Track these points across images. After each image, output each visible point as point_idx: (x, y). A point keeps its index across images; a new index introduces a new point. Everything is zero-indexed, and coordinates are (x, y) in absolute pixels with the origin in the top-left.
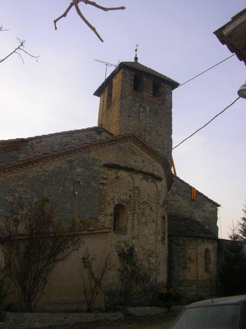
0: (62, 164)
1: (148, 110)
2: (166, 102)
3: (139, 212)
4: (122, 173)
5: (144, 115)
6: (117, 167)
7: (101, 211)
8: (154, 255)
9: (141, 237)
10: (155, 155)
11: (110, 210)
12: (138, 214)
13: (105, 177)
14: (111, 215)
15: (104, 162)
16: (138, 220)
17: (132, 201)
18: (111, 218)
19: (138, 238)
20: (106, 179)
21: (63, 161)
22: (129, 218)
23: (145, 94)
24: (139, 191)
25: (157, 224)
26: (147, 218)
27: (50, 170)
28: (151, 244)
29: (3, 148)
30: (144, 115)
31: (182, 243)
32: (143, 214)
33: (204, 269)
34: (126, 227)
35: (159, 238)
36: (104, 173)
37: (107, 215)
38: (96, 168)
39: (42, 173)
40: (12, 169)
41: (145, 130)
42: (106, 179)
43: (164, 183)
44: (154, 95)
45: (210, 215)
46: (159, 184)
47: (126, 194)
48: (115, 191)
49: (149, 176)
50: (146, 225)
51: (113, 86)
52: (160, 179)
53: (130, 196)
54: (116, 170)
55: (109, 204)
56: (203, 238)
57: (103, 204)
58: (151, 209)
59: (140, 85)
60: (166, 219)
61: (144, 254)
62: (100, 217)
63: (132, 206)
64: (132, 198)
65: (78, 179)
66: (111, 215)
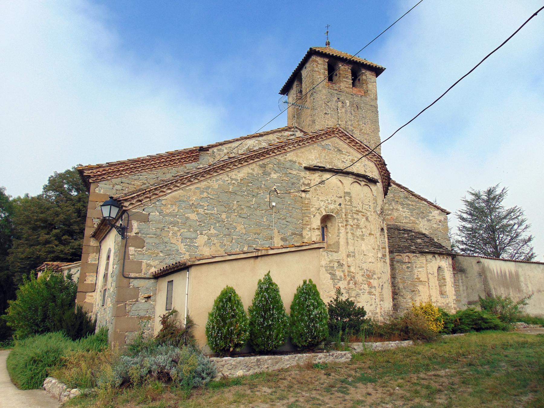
0: (253, 170)
1: (348, 104)
2: (369, 92)
3: (352, 224)
4: (327, 176)
5: (343, 110)
6: (323, 170)
7: (305, 224)
8: (375, 276)
9: (357, 255)
11: (316, 222)
12: (352, 226)
13: (306, 182)
14: (318, 229)
15: (304, 165)
16: (352, 234)
17: (344, 210)
18: (319, 233)
19: (354, 256)
20: (308, 184)
21: (254, 165)
22: (340, 231)
23: (343, 85)
24: (351, 197)
25: (376, 238)
26: (364, 230)
27: (239, 179)
28: (370, 262)
29: (178, 159)
30: (343, 110)
31: (407, 261)
32: (357, 225)
33: (438, 292)
34: (338, 243)
35: (380, 255)
36: (305, 178)
37: (314, 229)
38: (295, 173)
39: (229, 182)
40: (192, 180)
43: (380, 185)
44: (354, 85)
46: (373, 187)
47: (335, 201)
48: (321, 199)
49: (361, 179)
50: (363, 239)
51: (303, 79)
52: (373, 181)
53: (340, 205)
54: (320, 173)
55: (314, 216)
56: (434, 253)
57: (308, 217)
58: (367, 219)
59: (336, 75)
60: (386, 231)
61: (363, 275)
62: (305, 233)
63: (344, 216)
64: (343, 206)
65: (275, 187)
66: (318, 229)
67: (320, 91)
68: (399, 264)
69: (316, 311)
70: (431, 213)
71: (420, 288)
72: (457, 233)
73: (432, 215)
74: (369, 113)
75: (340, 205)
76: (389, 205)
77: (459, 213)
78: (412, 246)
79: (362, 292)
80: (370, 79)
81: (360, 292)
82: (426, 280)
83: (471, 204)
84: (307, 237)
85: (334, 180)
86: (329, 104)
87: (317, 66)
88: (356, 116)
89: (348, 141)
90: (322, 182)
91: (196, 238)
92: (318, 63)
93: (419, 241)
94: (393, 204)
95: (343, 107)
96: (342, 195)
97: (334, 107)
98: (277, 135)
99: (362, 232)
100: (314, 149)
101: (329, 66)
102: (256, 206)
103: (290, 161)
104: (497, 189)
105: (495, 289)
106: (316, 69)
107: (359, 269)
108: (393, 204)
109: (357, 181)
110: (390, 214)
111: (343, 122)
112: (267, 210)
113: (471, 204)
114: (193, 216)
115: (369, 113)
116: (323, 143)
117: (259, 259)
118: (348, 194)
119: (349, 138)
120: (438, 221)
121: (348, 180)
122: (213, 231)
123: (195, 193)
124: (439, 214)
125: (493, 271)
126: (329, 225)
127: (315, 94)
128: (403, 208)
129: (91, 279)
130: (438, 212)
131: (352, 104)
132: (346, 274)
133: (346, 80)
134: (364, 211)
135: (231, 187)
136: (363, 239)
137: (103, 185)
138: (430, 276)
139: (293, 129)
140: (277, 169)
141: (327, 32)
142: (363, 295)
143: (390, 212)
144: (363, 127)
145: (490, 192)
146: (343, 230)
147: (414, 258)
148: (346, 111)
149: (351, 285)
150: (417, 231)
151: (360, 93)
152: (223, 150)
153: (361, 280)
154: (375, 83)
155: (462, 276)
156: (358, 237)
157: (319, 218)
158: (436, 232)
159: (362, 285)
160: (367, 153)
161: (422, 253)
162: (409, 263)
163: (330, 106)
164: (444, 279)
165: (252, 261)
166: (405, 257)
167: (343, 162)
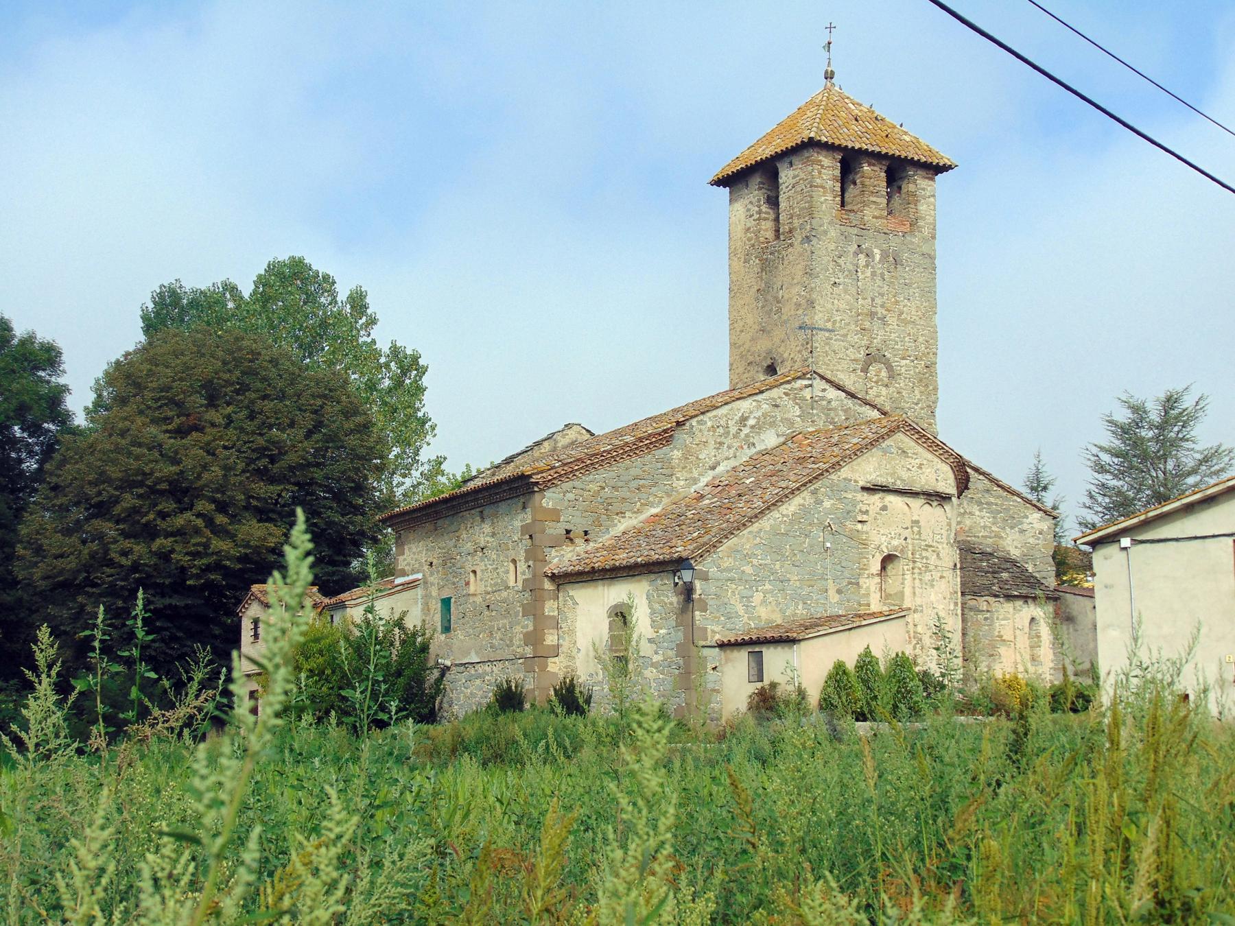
1: (878, 257)
2: (921, 223)
4: (891, 499)
7: (862, 569)
10: (941, 452)
12: (920, 569)
13: (864, 509)
15: (861, 483)
16: (921, 580)
17: (910, 547)
19: (922, 611)
20: (867, 512)
23: (869, 213)
24: (919, 527)
31: (985, 608)
34: (902, 593)
41: (872, 315)
42: (867, 512)
45: (1038, 539)
48: (882, 532)
50: (932, 586)
53: (906, 539)
54: (880, 495)
55: (873, 556)
62: (861, 581)
63: (910, 555)
64: (909, 541)
67: (825, 232)
68: (972, 613)
69: (912, 684)
70: (1027, 518)
71: (1002, 650)
72: (1084, 504)
75: (906, 539)
77: (1095, 450)
78: (993, 584)
81: (927, 659)
82: (1012, 638)
83: (1124, 431)
84: (865, 586)
85: (893, 500)
86: (840, 261)
87: (820, 173)
88: (892, 282)
89: (917, 436)
90: (884, 508)
91: (752, 597)
92: (822, 166)
93: (1005, 575)
95: (867, 266)
96: (909, 524)
97: (851, 267)
100: (872, 456)
101: (842, 162)
102: (809, 549)
103: (845, 479)
104: (1185, 398)
106: (818, 180)
112: (821, 553)
113: (1124, 431)
114: (748, 569)
116: (884, 445)
117: (853, 631)
118: (916, 522)
119: (918, 432)
121: (916, 503)
122: (768, 587)
123: (748, 539)
124: (1041, 520)
126: (889, 567)
127: (814, 241)
128: (980, 510)
129: (551, 638)
130: (1038, 515)
131: (885, 256)
132: (912, 635)
133: (874, 199)
134: (934, 544)
135: (782, 526)
136: (932, 586)
137: (551, 495)
138: (1018, 632)
139: (809, 376)
140: (830, 493)
141: (829, 43)
145: (1170, 402)
146: (908, 577)
147: (997, 604)
148: (874, 274)
149: (917, 650)
150: (1001, 554)
151: (903, 228)
152: (706, 423)
154: (932, 199)
155: (1068, 629)
157: (879, 558)
158: (1032, 552)
160: (941, 452)
161: (1009, 597)
162: (988, 611)
163: (843, 266)
164: (1039, 637)
165: (847, 633)
166: (982, 603)
167: (909, 469)
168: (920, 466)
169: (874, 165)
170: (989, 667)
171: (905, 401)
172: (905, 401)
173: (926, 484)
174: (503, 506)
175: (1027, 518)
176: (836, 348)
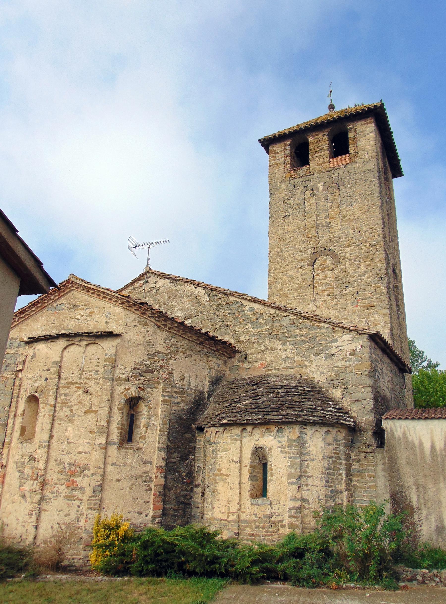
5: (313, 200)
53: (46, 379)
73: (338, 343)
74: (359, 185)
76: (260, 344)
79: (54, 496)
80: (363, 132)
94: (267, 341)
98: (129, 290)
99: (71, 411)
105: (418, 486)
107: (55, 463)
108: (267, 341)
109: (73, 343)
110: (260, 359)
111: (311, 219)
115: (359, 185)
120: (348, 354)
125: (421, 444)
128: (283, 344)
136: (71, 421)
141: (331, 92)
142: (56, 499)
143: (259, 356)
144: (347, 211)
153: (56, 479)
156: (62, 420)
159: (56, 486)
167: (78, 319)
168: (90, 315)
169: (317, 135)
170: (212, 514)
171: (351, 276)
172: (351, 276)
173: (95, 328)
174: (235, 427)
175: (336, 341)
176: (286, 256)
